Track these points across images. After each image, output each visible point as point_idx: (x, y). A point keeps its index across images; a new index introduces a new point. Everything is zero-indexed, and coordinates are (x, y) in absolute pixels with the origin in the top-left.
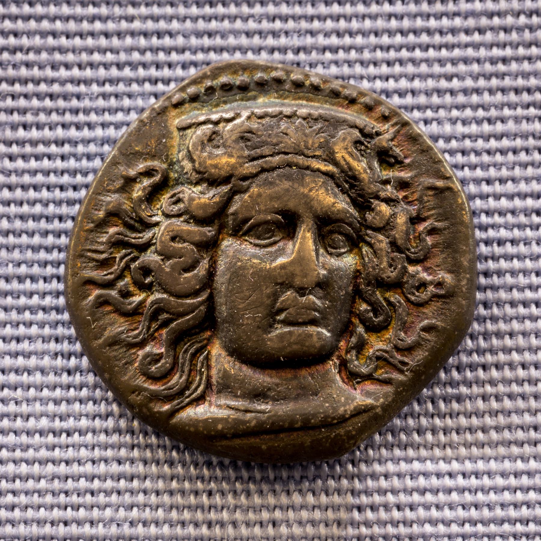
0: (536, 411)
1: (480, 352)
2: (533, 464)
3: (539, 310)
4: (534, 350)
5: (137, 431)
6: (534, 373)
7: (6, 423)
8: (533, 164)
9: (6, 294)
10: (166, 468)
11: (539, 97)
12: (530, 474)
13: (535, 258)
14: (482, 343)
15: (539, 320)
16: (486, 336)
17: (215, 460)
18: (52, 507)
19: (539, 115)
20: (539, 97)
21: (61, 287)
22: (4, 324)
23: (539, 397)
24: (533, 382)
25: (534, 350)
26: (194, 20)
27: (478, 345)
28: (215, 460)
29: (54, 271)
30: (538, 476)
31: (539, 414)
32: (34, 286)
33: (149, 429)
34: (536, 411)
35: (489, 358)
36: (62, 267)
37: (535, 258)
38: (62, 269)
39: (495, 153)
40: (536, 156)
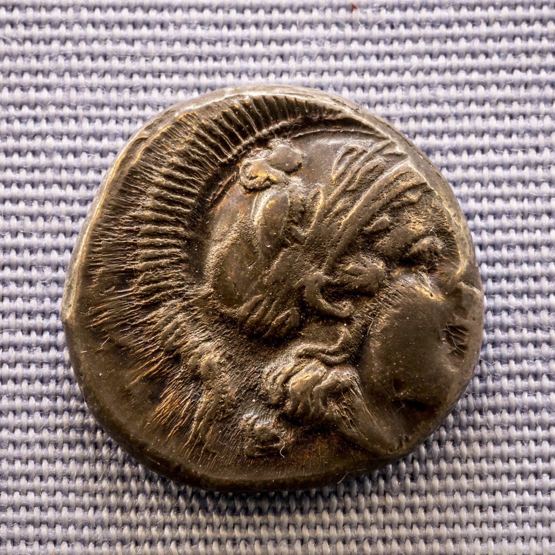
2: (546, 447)
3: (553, 544)
4: (548, 294)
5: (143, 475)
6: (546, 513)
7: (6, 304)
8: (546, 68)
9: (4, 136)
10: (173, 515)
12: (543, 21)
18: (58, 233)
19: (553, 48)
22: (4, 201)
23: (554, 184)
24: (545, 522)
25: (547, 459)
29: (52, 339)
31: (553, 199)
32: (32, 322)
33: (156, 475)
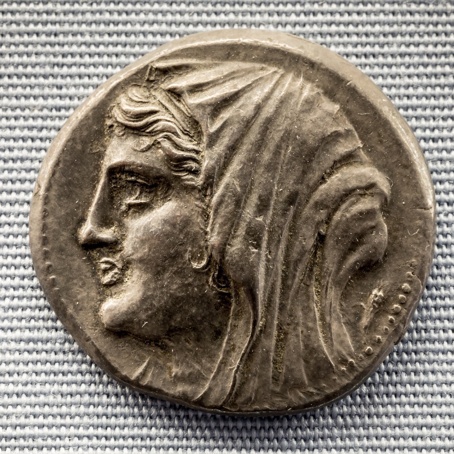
0: (452, 150)
1: (415, 342)
4: (450, 384)
11: (452, 59)
13: (449, 363)
14: (415, 335)
15: (452, 385)
16: (418, 330)
17: (191, 414)
20: (452, 59)
21: (28, 251)
25: (450, 384)
26: (222, 25)
27: (412, 337)
28: (191, 414)
30: (452, 406)
34: (452, 150)
35: (420, 346)
36: (28, 237)
37: (449, 363)
38: (28, 239)
39: (429, 140)
40: (451, 335)
